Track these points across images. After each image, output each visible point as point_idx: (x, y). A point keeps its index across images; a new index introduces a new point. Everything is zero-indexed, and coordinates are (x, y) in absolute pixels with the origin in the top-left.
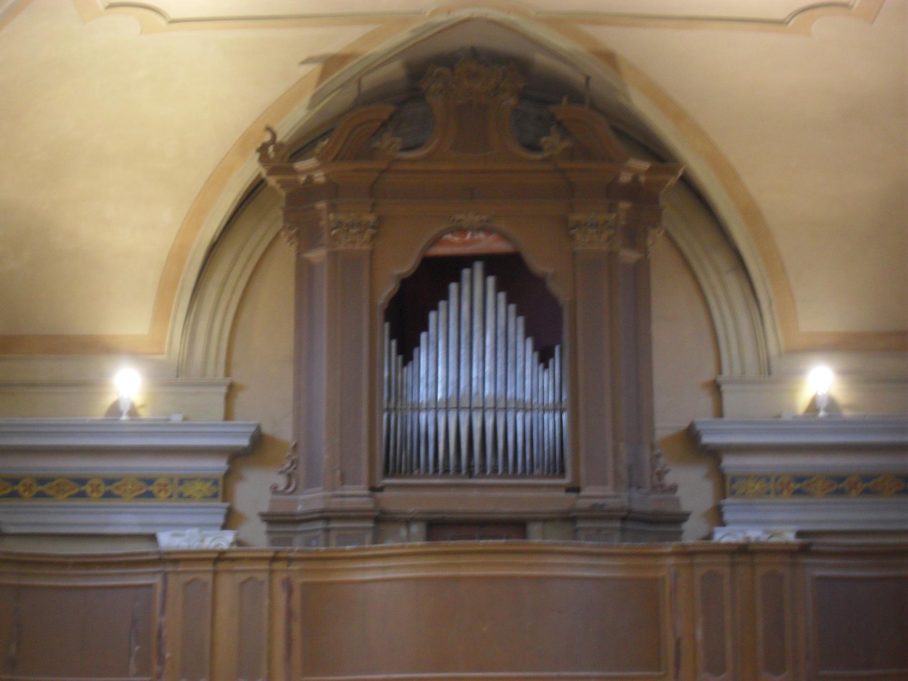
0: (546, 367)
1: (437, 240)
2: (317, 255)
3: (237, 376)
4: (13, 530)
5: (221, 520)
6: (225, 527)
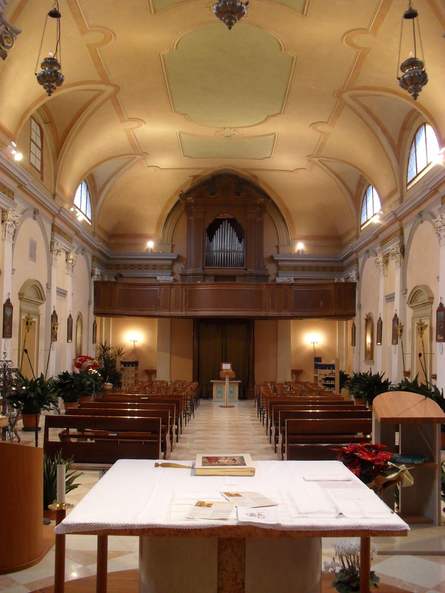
0: (241, 243)
1: (218, 215)
2: (192, 218)
3: (174, 243)
4: (126, 276)
5: (170, 274)
6: (171, 276)
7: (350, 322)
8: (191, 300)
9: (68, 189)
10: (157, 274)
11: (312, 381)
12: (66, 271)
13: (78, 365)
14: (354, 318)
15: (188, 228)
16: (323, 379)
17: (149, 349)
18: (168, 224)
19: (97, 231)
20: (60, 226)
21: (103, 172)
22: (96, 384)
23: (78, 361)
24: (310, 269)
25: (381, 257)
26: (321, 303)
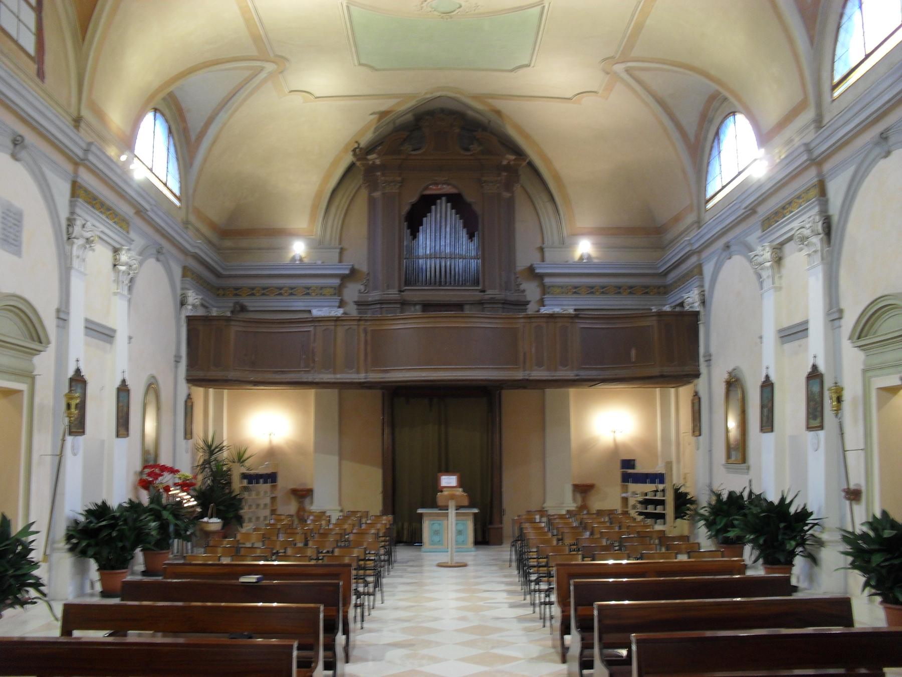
1: (426, 188)
2: (377, 194)
5: (337, 304)
6: (339, 307)
7: (685, 392)
8: (377, 350)
9: (116, 117)
10: (313, 304)
11: (617, 506)
12: (114, 288)
13: (145, 484)
14: (696, 381)
15: (369, 225)
16: (640, 502)
17: (299, 448)
18: (333, 210)
19: (193, 219)
20: (94, 193)
21: (200, 95)
22: (176, 525)
23: (145, 477)
24: (604, 290)
25: (768, 249)
26: (633, 352)
